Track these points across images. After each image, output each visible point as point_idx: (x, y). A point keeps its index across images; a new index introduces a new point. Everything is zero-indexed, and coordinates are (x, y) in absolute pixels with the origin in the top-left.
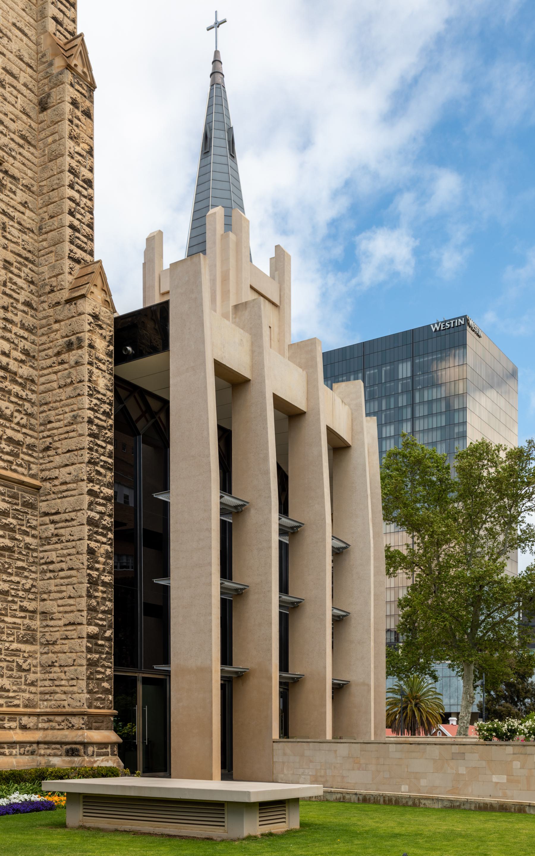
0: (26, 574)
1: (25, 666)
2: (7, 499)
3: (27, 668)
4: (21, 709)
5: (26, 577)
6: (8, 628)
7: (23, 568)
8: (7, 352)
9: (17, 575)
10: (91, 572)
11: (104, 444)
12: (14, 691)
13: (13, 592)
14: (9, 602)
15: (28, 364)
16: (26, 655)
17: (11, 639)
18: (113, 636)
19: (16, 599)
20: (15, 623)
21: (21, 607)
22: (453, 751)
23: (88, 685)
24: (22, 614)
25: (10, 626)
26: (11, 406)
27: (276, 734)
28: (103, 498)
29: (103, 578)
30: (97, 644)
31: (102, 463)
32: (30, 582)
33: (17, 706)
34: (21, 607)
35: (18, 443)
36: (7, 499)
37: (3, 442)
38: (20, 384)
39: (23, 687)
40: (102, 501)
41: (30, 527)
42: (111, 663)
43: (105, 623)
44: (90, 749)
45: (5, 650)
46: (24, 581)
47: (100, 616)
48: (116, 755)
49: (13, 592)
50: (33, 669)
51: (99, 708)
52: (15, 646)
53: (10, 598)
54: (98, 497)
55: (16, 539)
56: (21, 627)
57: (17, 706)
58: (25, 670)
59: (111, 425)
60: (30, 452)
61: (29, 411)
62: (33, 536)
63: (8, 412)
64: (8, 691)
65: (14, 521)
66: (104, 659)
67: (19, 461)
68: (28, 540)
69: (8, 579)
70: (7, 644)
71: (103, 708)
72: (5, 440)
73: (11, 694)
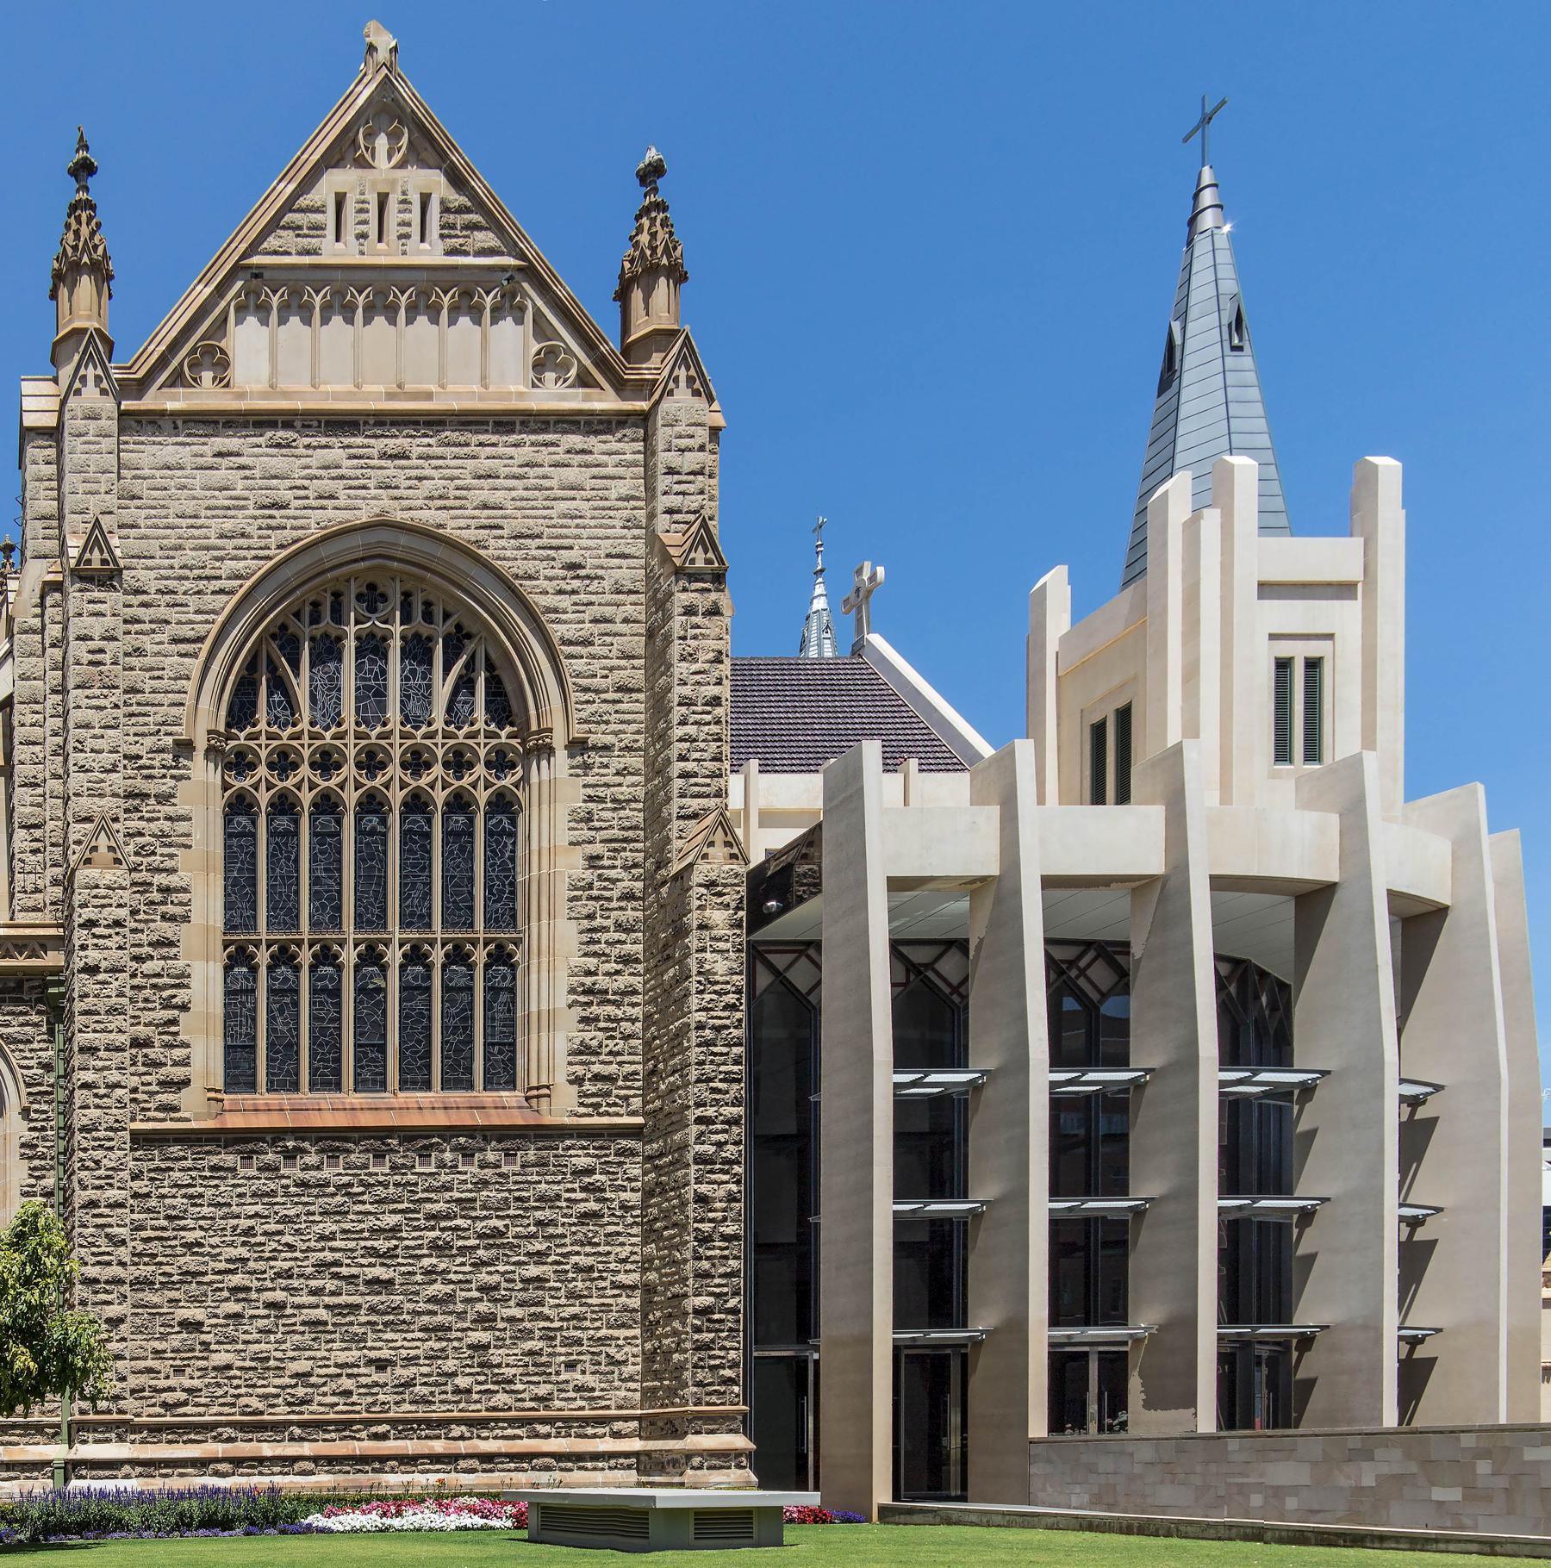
0: (621, 1239)
1: (619, 1357)
2: (592, 1151)
3: (624, 1358)
4: (613, 1412)
5: (622, 1244)
6: (593, 1312)
7: (618, 1234)
8: (593, 969)
9: (608, 1244)
10: (700, 1226)
11: (725, 1050)
12: (602, 1390)
13: (601, 1266)
14: (595, 1279)
15: (627, 972)
16: (621, 1342)
17: (598, 1324)
18: (741, 1306)
19: (605, 1274)
20: (603, 1305)
21: (612, 1282)
22: (1350, 1446)
23: (694, 1374)
24: (616, 1292)
25: (597, 1309)
26: (600, 1034)
27: (1038, 1426)
28: (722, 1123)
29: (722, 1229)
30: (709, 1320)
31: (721, 1076)
32: (628, 1249)
33: (608, 1407)
34: (612, 1282)
35: (610, 1079)
36: (592, 1151)
37: (587, 1083)
38: (614, 1003)
39: (617, 1383)
40: (719, 1127)
41: (628, 1179)
42: (738, 1342)
43: (725, 1290)
44: (696, 1461)
45: (588, 1339)
46: (619, 1249)
47: (717, 1281)
48: (744, 1467)
49: (601, 1266)
50: (632, 1360)
51: (714, 1404)
52: (603, 1332)
53: (596, 1275)
54: (714, 1123)
55: (607, 1199)
56: (614, 1308)
57: (608, 1407)
58: (619, 1363)
59: (740, 1021)
60: (629, 1084)
61: (627, 1032)
62: (633, 1190)
63: (594, 1043)
64: (593, 1390)
65: (603, 1178)
66: (725, 1339)
67: (611, 1100)
68: (623, 1196)
69: (164, 1395)
70: (592, 1332)
71: (722, 1404)
72: (589, 1079)
73: (597, 1394)
